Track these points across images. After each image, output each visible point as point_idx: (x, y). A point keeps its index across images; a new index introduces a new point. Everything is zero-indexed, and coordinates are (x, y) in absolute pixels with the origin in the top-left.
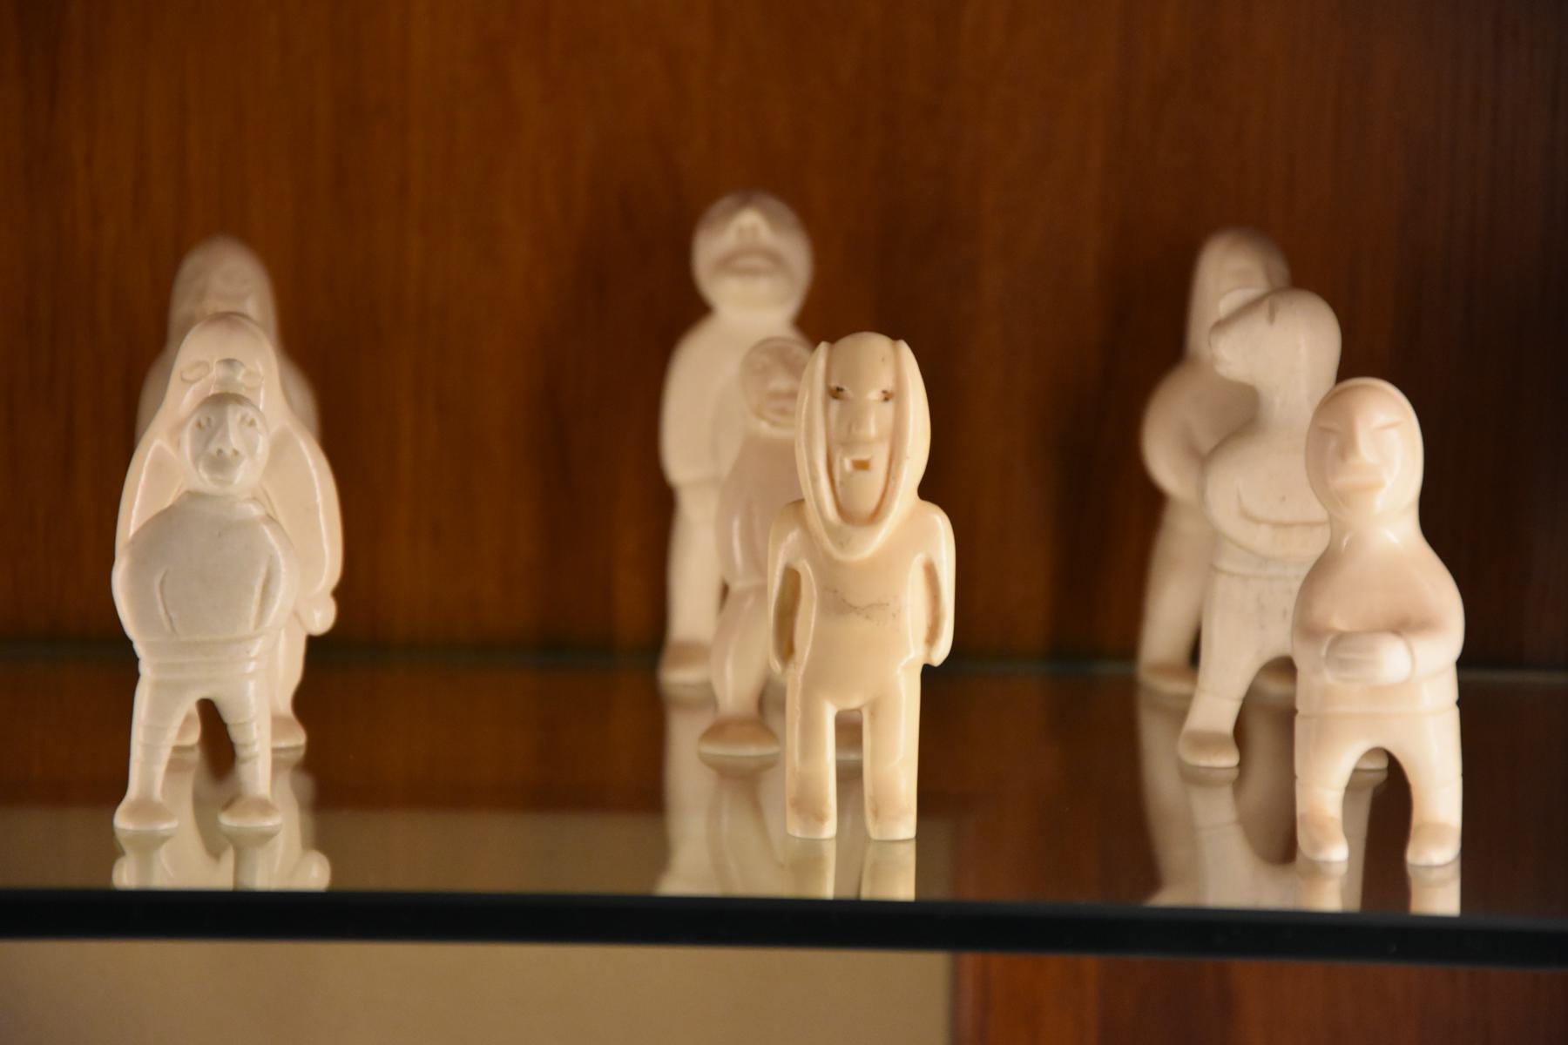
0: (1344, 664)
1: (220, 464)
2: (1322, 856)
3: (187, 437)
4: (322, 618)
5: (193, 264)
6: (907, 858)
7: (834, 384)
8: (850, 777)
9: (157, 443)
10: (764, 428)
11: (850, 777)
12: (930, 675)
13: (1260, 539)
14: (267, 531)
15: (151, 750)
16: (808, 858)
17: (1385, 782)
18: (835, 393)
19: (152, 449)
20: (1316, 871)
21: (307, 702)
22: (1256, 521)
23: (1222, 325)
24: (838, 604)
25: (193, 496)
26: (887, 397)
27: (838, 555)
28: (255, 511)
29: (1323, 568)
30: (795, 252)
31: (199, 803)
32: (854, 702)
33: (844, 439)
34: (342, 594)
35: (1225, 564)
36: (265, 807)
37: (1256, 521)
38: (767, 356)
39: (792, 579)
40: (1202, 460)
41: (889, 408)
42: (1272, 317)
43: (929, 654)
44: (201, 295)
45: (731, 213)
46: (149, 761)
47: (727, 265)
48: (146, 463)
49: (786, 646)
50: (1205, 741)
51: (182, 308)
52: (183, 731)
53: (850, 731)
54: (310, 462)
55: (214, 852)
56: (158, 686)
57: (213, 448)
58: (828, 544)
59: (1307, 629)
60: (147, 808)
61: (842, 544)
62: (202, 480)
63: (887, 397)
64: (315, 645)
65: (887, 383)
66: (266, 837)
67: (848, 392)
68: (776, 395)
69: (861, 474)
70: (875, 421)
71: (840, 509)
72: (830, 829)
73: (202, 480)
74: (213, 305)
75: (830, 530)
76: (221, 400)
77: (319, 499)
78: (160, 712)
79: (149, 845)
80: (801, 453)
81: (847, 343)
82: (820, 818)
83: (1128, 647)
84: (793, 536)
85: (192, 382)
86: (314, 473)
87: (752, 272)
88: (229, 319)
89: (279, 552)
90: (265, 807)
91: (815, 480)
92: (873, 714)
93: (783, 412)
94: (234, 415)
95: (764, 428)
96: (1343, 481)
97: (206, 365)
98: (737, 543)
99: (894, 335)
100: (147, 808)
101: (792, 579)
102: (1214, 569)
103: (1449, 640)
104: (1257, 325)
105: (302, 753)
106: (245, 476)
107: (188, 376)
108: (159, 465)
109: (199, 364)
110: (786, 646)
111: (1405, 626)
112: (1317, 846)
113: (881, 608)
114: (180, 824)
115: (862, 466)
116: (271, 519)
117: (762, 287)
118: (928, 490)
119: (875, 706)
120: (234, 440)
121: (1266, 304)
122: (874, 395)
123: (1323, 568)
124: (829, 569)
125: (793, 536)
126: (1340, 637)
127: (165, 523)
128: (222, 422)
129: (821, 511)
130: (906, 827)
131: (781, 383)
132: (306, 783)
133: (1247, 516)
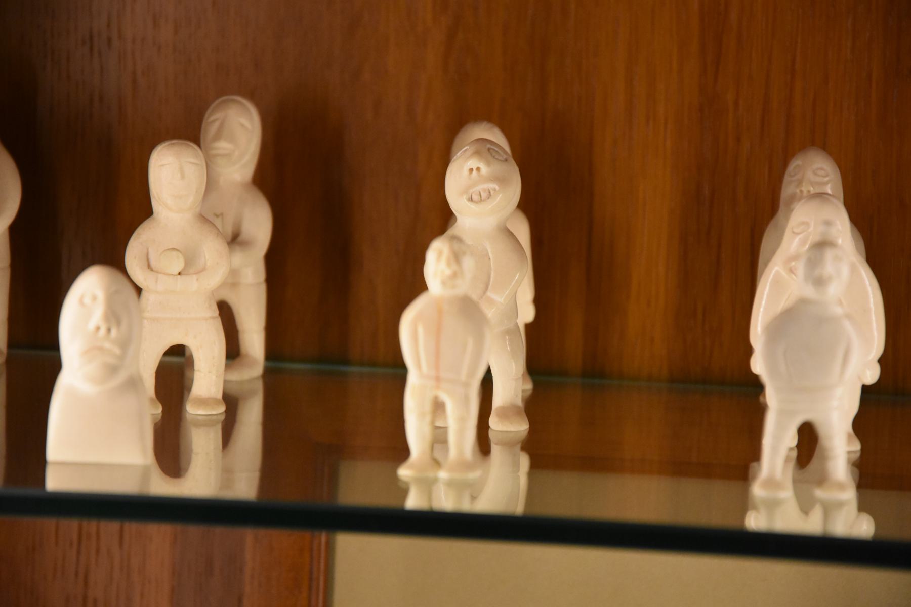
1: (820, 282)
3: (800, 267)
4: (872, 376)
9: (776, 268)
15: (775, 449)
17: (527, 435)
19: (774, 272)
21: (860, 425)
25: (803, 302)
28: (838, 310)
30: (496, 136)
31: (795, 481)
34: (882, 361)
36: (841, 486)
44: (800, 183)
48: (770, 280)
51: (787, 190)
54: (867, 283)
55: (805, 509)
62: (809, 292)
66: (840, 505)
73: (809, 292)
74: (807, 188)
76: (822, 245)
77: (872, 305)
79: (773, 505)
85: (798, 234)
86: (869, 289)
88: (820, 196)
90: (841, 486)
94: (829, 254)
97: (807, 224)
105: (858, 455)
106: (834, 290)
107: (796, 230)
108: (777, 281)
109: (803, 223)
116: (848, 316)
132: (857, 471)
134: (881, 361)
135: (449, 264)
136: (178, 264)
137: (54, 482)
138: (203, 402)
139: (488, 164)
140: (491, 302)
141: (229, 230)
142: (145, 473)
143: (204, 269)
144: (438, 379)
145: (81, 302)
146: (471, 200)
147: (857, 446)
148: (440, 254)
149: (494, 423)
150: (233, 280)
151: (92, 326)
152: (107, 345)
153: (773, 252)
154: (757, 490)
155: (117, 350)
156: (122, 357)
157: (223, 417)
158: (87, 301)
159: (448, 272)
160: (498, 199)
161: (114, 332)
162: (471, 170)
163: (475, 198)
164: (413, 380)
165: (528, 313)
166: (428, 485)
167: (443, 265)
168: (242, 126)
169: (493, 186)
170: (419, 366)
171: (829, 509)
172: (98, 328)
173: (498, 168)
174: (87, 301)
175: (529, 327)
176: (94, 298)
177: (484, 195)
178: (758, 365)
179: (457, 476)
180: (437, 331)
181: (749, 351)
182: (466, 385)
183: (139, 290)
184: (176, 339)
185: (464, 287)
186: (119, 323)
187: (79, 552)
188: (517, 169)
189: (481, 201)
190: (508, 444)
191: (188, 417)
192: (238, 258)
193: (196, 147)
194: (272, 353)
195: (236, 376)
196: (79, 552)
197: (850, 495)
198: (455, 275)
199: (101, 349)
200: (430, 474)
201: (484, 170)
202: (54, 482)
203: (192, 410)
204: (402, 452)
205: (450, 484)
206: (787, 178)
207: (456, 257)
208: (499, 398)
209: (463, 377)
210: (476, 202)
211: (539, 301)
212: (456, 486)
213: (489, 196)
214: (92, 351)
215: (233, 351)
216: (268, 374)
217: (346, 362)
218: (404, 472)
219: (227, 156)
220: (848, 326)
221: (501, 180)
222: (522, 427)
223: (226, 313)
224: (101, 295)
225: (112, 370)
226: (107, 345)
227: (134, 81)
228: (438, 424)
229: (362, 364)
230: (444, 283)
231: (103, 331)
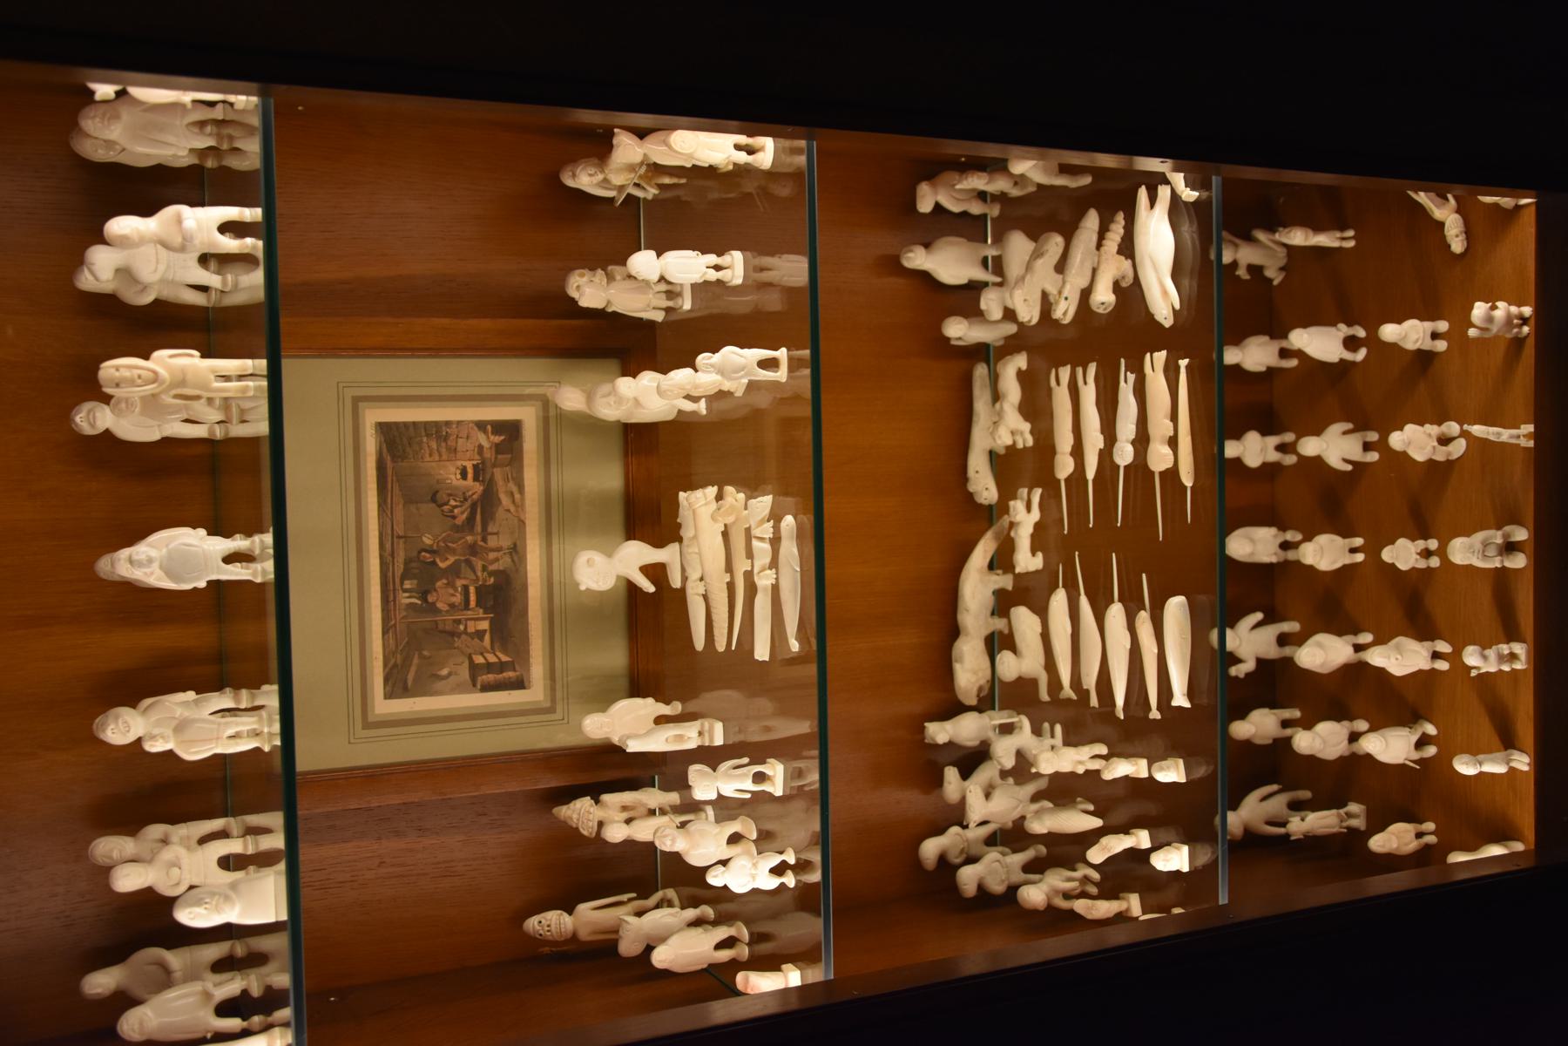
0: (192, 238)
1: (150, 561)
2: (250, 245)
4: (202, 532)
5: (102, 575)
6: (257, 362)
7: (114, 385)
8: (241, 377)
10: (137, 410)
11: (241, 377)
12: (203, 356)
13: (162, 268)
14: (170, 547)
16: (257, 389)
18: (117, 385)
20: (254, 247)
22: (156, 269)
23: (97, 279)
24: (183, 383)
25: (161, 567)
26: (117, 370)
27: (167, 383)
28: (164, 550)
29: (165, 245)
32: (212, 377)
33: (131, 382)
35: (171, 278)
36: (253, 542)
37: (156, 269)
38: (117, 413)
39: (177, 396)
40: (145, 288)
41: (121, 370)
42: (93, 264)
43: (197, 356)
45: (76, 425)
46: (242, 575)
47: (93, 426)
49: (198, 398)
50: (224, 282)
52: (237, 567)
53: (227, 378)
56: (218, 573)
57: (145, 562)
58: (164, 386)
59: (182, 249)
60: (255, 574)
61: (163, 382)
62: (156, 565)
63: (117, 370)
64: (209, 534)
65: (113, 370)
67: (117, 381)
68: (127, 407)
69: (143, 377)
70: (126, 373)
71: (153, 382)
72: (251, 384)
73: (156, 565)
75: (161, 384)
76: (131, 561)
78: (232, 573)
79: (264, 572)
80: (142, 394)
81: (102, 382)
82: (247, 386)
83: (206, 309)
84: (163, 397)
87: (94, 418)
89: (181, 541)
90: (253, 542)
91: (144, 391)
92: (216, 372)
93: (132, 405)
94: (135, 557)
95: (137, 410)
96: (137, 240)
98: (173, 417)
99: (98, 369)
100: (255, 574)
101: (177, 396)
102: (172, 281)
103: (184, 210)
104: (94, 268)
106: (153, 553)
110: (198, 398)
111: (179, 220)
112: (247, 247)
113: (183, 371)
114: (258, 566)
115: (139, 377)
116: (167, 546)
117: (98, 415)
118: (147, 357)
119: (213, 371)
120: (143, 557)
121: (91, 266)
122: (117, 374)
123: (165, 245)
124: (173, 385)
125: (163, 397)
126: (184, 239)
127: (170, 574)
128: (138, 561)
129: (152, 389)
130: (249, 362)
131: (123, 405)
133: (155, 271)
134: (194, 528)
135: (157, 741)
136: (175, 871)
137: (284, 917)
138: (245, 846)
139: (109, 725)
140: (181, 715)
141: (160, 845)
142: (277, 873)
143: (177, 857)
144: (218, 738)
145: (192, 919)
146: (128, 731)
147: (238, 536)
148: (151, 746)
149: (243, 706)
150: (184, 842)
151: (203, 912)
152: (214, 903)
153: (146, 583)
154: (259, 580)
155: (217, 897)
156: (220, 894)
157: (253, 836)
158: (192, 916)
159: (161, 741)
160: (127, 718)
161: (207, 900)
162: (113, 733)
163: (127, 729)
164: (219, 751)
165: (191, 695)
166: (271, 735)
167: (157, 744)
168: (103, 847)
169: (120, 721)
170: (212, 748)
171: (263, 548)
172: (206, 908)
173: (110, 720)
174: (192, 916)
175: (1100, 450)
176: (190, 913)
177: (126, 725)
178: (202, 584)
179: (265, 722)
180: (193, 742)
181: (195, 589)
182: (219, 724)
183: (192, 887)
184: (214, 864)
185: (169, 732)
186: (202, 899)
187: (330, 888)
188: (116, 709)
189: (129, 726)
190: (253, 697)
191: (254, 852)
192: (174, 839)
193: (115, 869)
194: (225, 814)
195: (235, 832)
196: (330, 888)
197: (257, 538)
198: (163, 737)
199: (216, 906)
200: (266, 736)
201: (112, 726)
202: (284, 917)
203: (250, 851)
204: (257, 750)
205: (270, 725)
206: (110, 579)
207: (153, 737)
208: (231, 705)
209: (215, 726)
210: (130, 729)
211: (184, 690)
212: (270, 725)
213: (126, 722)
214: (218, 910)
215: (223, 834)
216: (234, 815)
217: (225, 777)
218: (267, 749)
219: (120, 851)
220: (170, 547)
221: (117, 718)
222: (244, 693)
223: (203, 840)
224: (188, 910)
225: (227, 898)
226: (214, 903)
227: (88, 901)
228: (246, 735)
229: (226, 769)
230: (167, 742)
231: (207, 906)
